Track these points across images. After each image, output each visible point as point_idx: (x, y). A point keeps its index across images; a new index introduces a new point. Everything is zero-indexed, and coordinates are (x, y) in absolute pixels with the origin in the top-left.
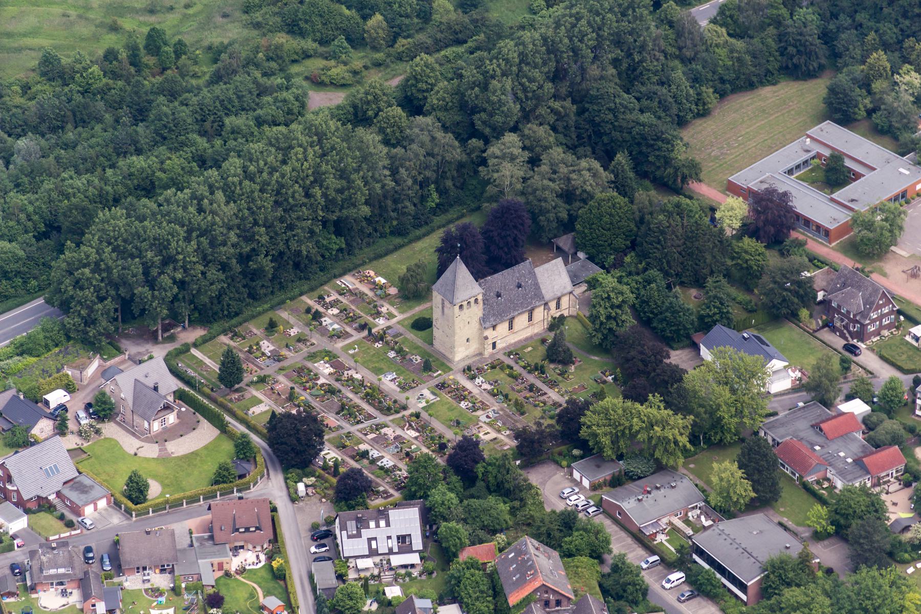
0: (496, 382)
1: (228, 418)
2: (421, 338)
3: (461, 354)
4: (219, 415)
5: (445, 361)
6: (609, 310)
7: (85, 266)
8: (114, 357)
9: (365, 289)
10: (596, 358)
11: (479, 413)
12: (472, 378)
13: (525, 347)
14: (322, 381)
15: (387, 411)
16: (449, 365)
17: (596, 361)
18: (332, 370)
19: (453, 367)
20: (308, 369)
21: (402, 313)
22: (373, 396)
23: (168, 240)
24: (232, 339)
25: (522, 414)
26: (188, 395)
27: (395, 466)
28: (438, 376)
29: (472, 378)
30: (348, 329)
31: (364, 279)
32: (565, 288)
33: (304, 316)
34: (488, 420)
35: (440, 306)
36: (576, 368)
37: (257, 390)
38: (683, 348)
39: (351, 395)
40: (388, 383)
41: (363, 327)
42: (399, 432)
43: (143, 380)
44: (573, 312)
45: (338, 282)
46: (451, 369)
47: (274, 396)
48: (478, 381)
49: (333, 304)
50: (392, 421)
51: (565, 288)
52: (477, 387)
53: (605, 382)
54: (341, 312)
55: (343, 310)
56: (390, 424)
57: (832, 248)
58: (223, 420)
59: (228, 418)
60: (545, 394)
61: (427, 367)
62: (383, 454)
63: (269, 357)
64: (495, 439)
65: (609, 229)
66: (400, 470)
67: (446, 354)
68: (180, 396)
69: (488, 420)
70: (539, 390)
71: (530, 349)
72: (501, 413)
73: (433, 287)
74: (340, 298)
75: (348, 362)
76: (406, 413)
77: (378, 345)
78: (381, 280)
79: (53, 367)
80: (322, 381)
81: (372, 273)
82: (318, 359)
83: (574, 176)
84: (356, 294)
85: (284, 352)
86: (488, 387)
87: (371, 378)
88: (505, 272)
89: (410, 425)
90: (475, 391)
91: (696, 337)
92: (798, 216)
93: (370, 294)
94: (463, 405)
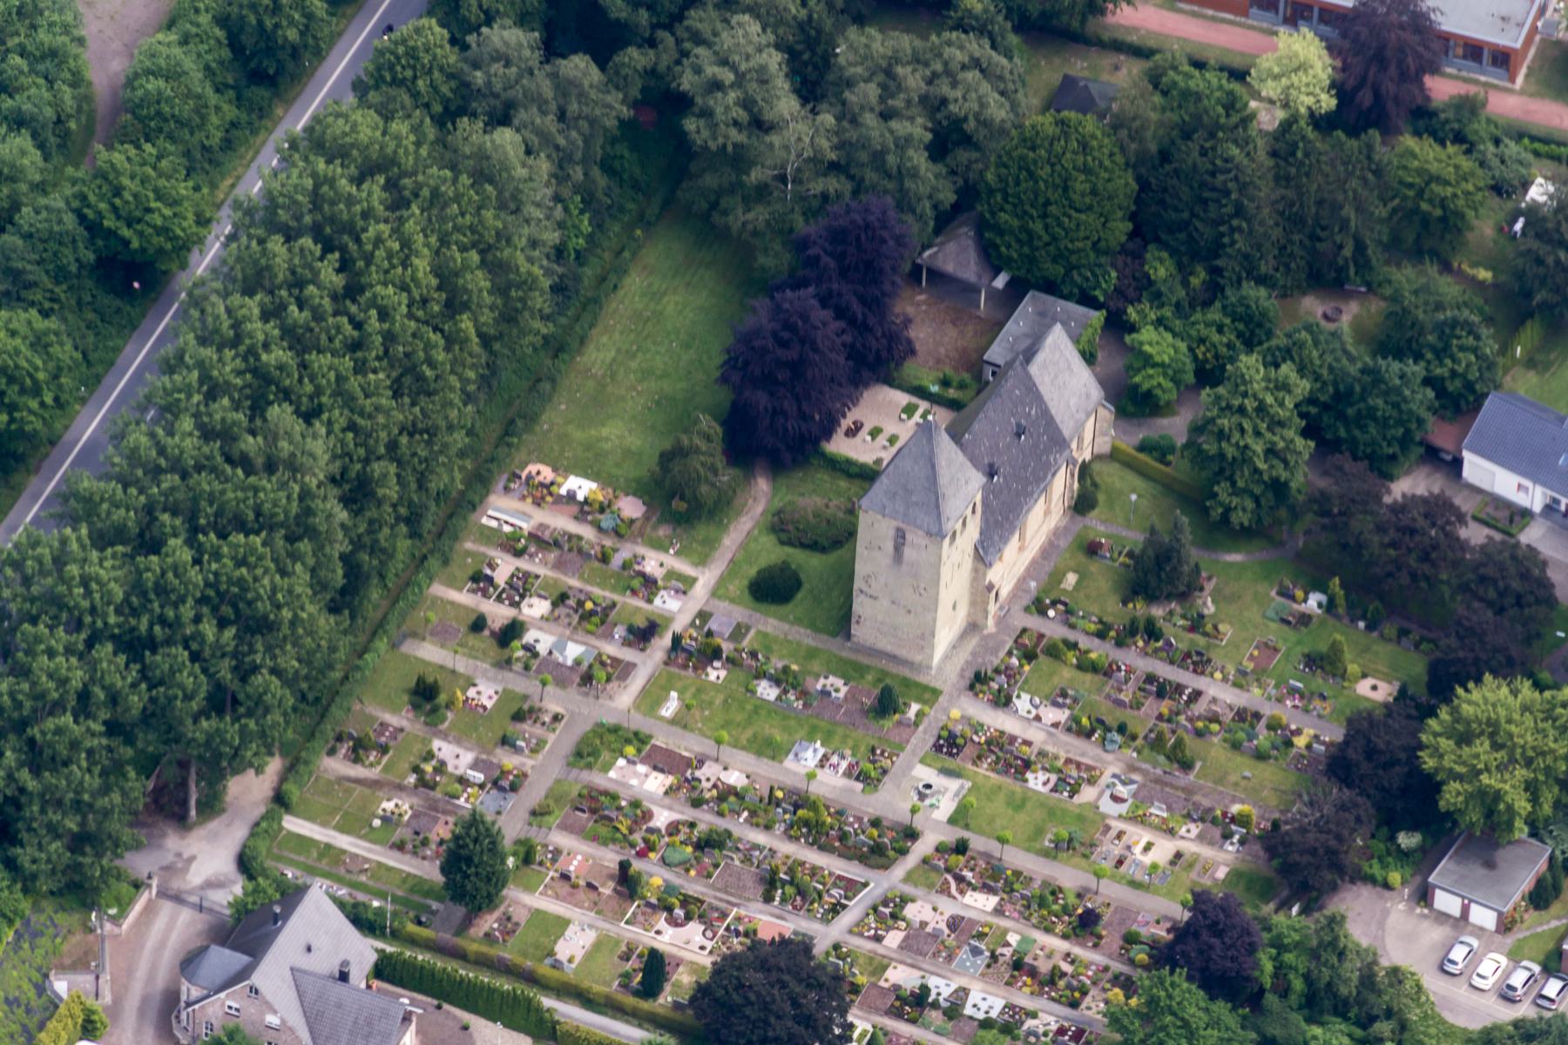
0: (1064, 695)
1: (547, 1002)
2: (798, 621)
3: (944, 648)
4: (529, 1001)
5: (906, 673)
6: (1268, 435)
7: (57, 707)
8: (131, 901)
9: (561, 522)
10: (1235, 557)
11: (1087, 794)
12: (1003, 701)
13: (1057, 577)
14: (662, 818)
15: (877, 856)
16: (922, 679)
17: (1240, 567)
18: (669, 780)
19: (937, 685)
20: (606, 793)
21: (702, 561)
22: (806, 816)
23: (241, 582)
24: (357, 760)
25: (1186, 766)
26: (432, 973)
27: (1009, 1007)
28: (924, 720)
29: (1003, 701)
30: (611, 649)
31: (541, 494)
32: (1088, 396)
33: (473, 640)
34: (1123, 809)
35: (889, 546)
36: (1217, 596)
37: (530, 889)
38: (1408, 473)
39: (760, 837)
40: (813, 768)
41: (643, 635)
42: (949, 908)
43: (305, 962)
44: (1104, 446)
45: (484, 520)
46: (936, 693)
47: (582, 895)
48: (1022, 703)
49: (520, 588)
50: (908, 878)
51: (1088, 396)
52: (1030, 720)
53: (1305, 619)
54: (555, 605)
55: (560, 599)
56: (908, 889)
57: (1522, 92)
58: (539, 1009)
59: (547, 1002)
60: (1197, 694)
61: (886, 705)
62: (962, 981)
63: (481, 786)
64: (1178, 855)
65: (1090, 208)
66: (1034, 1015)
67: (903, 653)
68: (384, 970)
69: (1123, 809)
70: (1179, 688)
71: (1071, 579)
72: (1136, 777)
73: (865, 502)
74: (524, 564)
75: (687, 745)
76: (923, 847)
77: (716, 673)
78: (582, 486)
79: (26, 986)
80: (662, 818)
81: (547, 474)
82: (605, 755)
83: (945, 89)
84: (557, 544)
85: (509, 761)
86: (1062, 715)
87: (767, 771)
88: (1058, 419)
89: (960, 879)
90: (1036, 735)
91: (1441, 434)
92: (1446, 38)
93: (587, 532)
94: (1037, 781)
